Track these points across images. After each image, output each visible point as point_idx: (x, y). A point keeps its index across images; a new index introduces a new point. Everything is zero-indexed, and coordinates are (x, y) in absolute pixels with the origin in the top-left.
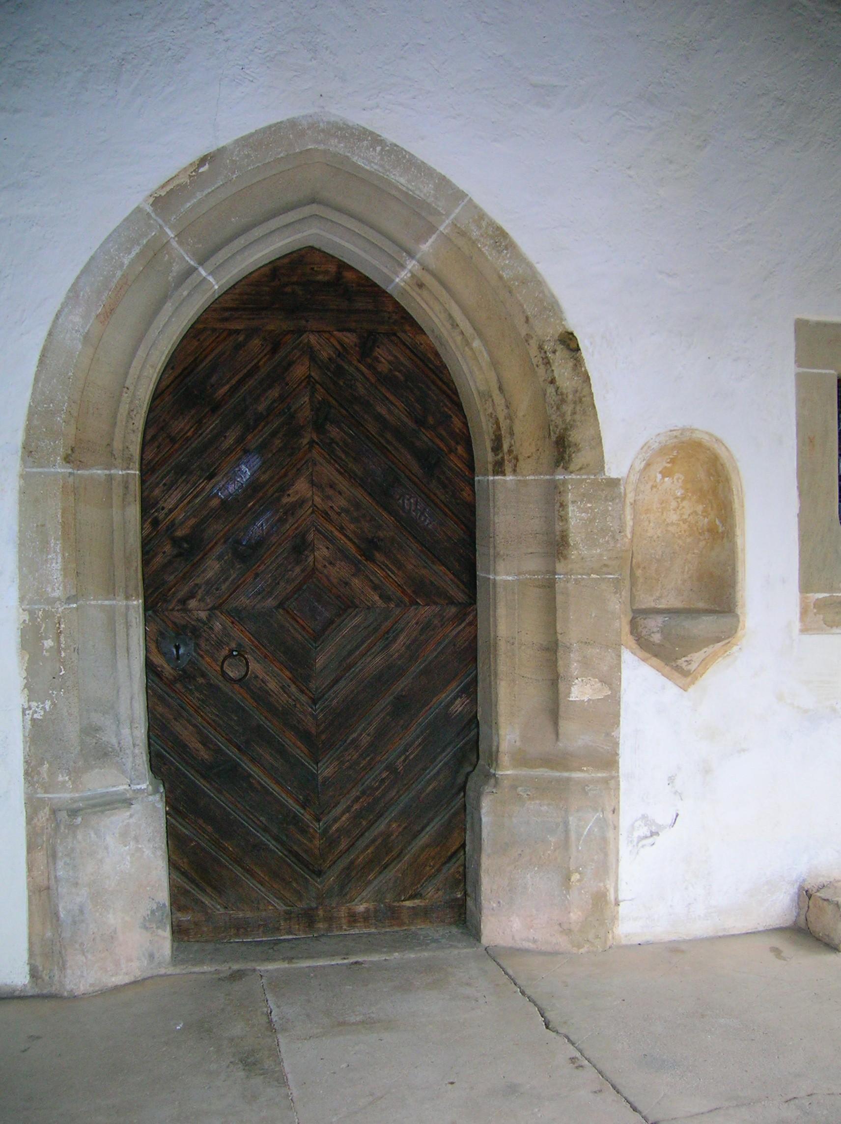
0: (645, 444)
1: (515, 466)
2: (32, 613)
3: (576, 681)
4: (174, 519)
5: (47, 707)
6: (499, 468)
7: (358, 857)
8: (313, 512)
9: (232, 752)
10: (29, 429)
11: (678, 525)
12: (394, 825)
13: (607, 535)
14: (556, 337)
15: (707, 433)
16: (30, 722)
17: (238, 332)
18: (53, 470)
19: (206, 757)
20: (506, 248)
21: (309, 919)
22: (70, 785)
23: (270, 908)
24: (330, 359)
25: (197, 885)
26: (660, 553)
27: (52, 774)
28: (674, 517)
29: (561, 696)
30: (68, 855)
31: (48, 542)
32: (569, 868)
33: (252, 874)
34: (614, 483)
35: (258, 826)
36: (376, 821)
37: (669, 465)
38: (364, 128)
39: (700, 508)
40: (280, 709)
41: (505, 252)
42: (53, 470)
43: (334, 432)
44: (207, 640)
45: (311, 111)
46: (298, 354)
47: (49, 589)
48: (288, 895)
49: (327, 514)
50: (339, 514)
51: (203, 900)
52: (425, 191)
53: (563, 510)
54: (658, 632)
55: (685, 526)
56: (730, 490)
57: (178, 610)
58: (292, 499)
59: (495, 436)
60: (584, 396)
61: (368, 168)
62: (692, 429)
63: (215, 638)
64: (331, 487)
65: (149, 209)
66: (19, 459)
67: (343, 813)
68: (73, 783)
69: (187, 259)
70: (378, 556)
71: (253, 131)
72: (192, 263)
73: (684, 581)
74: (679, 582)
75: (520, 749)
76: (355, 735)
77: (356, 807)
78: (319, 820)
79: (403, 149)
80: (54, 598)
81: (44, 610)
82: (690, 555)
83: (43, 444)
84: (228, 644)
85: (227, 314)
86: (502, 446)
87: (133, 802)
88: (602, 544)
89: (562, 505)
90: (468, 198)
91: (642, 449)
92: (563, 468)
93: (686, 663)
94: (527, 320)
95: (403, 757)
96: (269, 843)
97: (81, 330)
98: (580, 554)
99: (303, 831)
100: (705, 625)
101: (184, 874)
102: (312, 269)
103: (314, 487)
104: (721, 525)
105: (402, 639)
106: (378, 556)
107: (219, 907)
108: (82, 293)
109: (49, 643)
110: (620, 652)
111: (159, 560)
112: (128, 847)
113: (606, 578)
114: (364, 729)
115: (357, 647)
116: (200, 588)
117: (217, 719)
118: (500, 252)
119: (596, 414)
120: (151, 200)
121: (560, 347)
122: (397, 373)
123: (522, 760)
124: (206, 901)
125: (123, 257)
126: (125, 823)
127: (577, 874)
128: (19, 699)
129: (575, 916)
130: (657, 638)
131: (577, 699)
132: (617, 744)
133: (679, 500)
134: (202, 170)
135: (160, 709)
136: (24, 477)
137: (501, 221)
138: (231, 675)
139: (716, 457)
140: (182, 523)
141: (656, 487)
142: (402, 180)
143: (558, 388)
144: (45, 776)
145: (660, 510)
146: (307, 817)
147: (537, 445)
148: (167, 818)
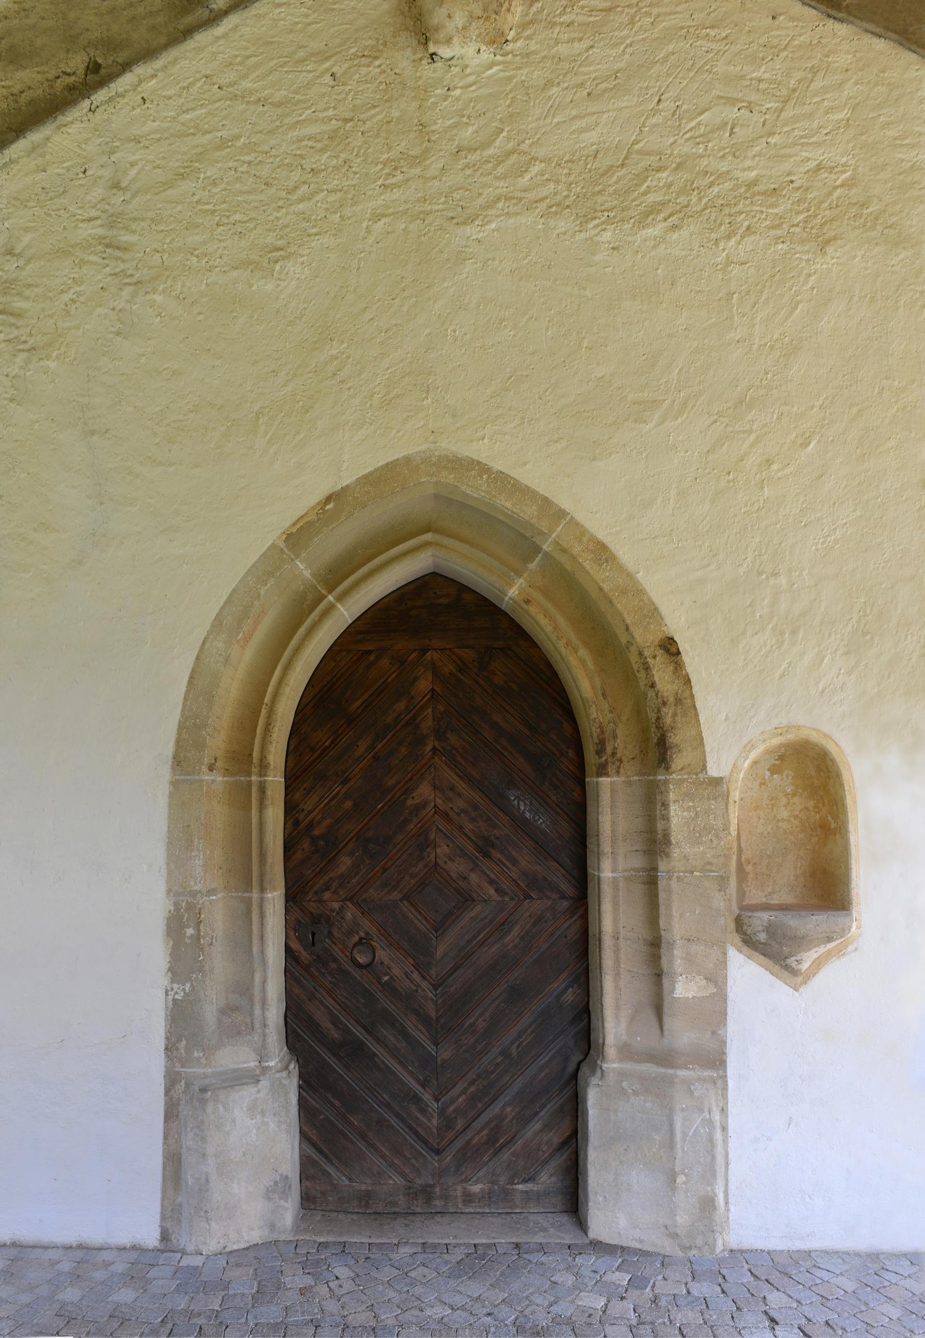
0: (749, 743)
1: (619, 767)
2: (176, 904)
3: (680, 978)
4: (313, 820)
5: (187, 991)
6: (602, 770)
7: (472, 1138)
8: (436, 812)
9: (359, 1032)
10: (178, 742)
11: (789, 821)
12: (508, 1109)
13: (710, 832)
14: (656, 643)
15: (814, 729)
16: (171, 1002)
17: (369, 652)
18: (197, 777)
19: (336, 1036)
20: (607, 561)
21: (426, 1194)
22: (203, 1061)
23: (391, 1182)
24: (450, 674)
25: (326, 1157)
26: (771, 849)
27: (188, 1050)
28: (785, 814)
29: (666, 992)
30: (197, 1127)
31: (192, 842)
32: (674, 1169)
33: (376, 1150)
34: (717, 782)
35: (382, 1103)
36: (490, 1104)
37: (777, 762)
38: (471, 459)
39: (811, 804)
40: (403, 993)
41: (605, 564)
42: (197, 777)
43: (453, 739)
44: (339, 929)
45: (424, 447)
46: (423, 670)
47: (192, 883)
48: (407, 1171)
49: (447, 814)
50: (458, 814)
51: (330, 1171)
52: (529, 513)
53: (665, 810)
54: (763, 931)
55: (796, 822)
56: (842, 785)
57: (314, 901)
58: (416, 801)
59: (599, 739)
60: (685, 699)
61: (475, 495)
62: (799, 726)
63: (346, 927)
64: (451, 789)
65: (282, 545)
66: (170, 767)
67: (460, 1095)
68: (207, 1059)
69: (320, 588)
70: (496, 854)
71: (372, 469)
72: (323, 592)
73: (797, 877)
74: (792, 878)
75: (626, 1042)
76: (472, 1021)
77: (472, 1089)
78: (437, 1100)
79: (507, 475)
80: (196, 890)
81: (187, 901)
82: (802, 851)
83: (190, 755)
84: (358, 933)
85: (360, 637)
86: (605, 749)
87: (261, 1078)
88: (705, 842)
89: (663, 804)
90: (570, 516)
91: (745, 747)
92: (664, 768)
93: (796, 963)
94: (627, 629)
95: (517, 1043)
96: (391, 1120)
97: (224, 654)
98: (683, 852)
99: (423, 1111)
100: (817, 922)
101: (314, 1145)
102: (435, 593)
103: (437, 791)
104: (833, 821)
105: (516, 931)
106: (496, 854)
107: (344, 1178)
108: (225, 622)
109: (190, 931)
110: (726, 949)
111: (299, 856)
112: (254, 1121)
113: (710, 876)
114: (480, 1015)
115: (475, 937)
116: (334, 881)
117: (346, 1001)
118: (600, 565)
119: (697, 715)
120: (284, 536)
121: (659, 653)
122: (512, 684)
123: (627, 1053)
124: (331, 1170)
125: (260, 588)
126: (253, 1098)
127: (683, 1176)
128: (163, 980)
129: (682, 1220)
130: (762, 937)
131: (681, 996)
132: (725, 1042)
133: (789, 796)
134: (328, 507)
135: (297, 991)
136: (174, 784)
137: (601, 535)
138: (360, 960)
139: (826, 754)
140: (320, 822)
141: (764, 784)
142: (508, 505)
143: (658, 691)
144: (183, 1051)
145: (770, 807)
146: (427, 1097)
147: (640, 747)
148: (299, 1092)
